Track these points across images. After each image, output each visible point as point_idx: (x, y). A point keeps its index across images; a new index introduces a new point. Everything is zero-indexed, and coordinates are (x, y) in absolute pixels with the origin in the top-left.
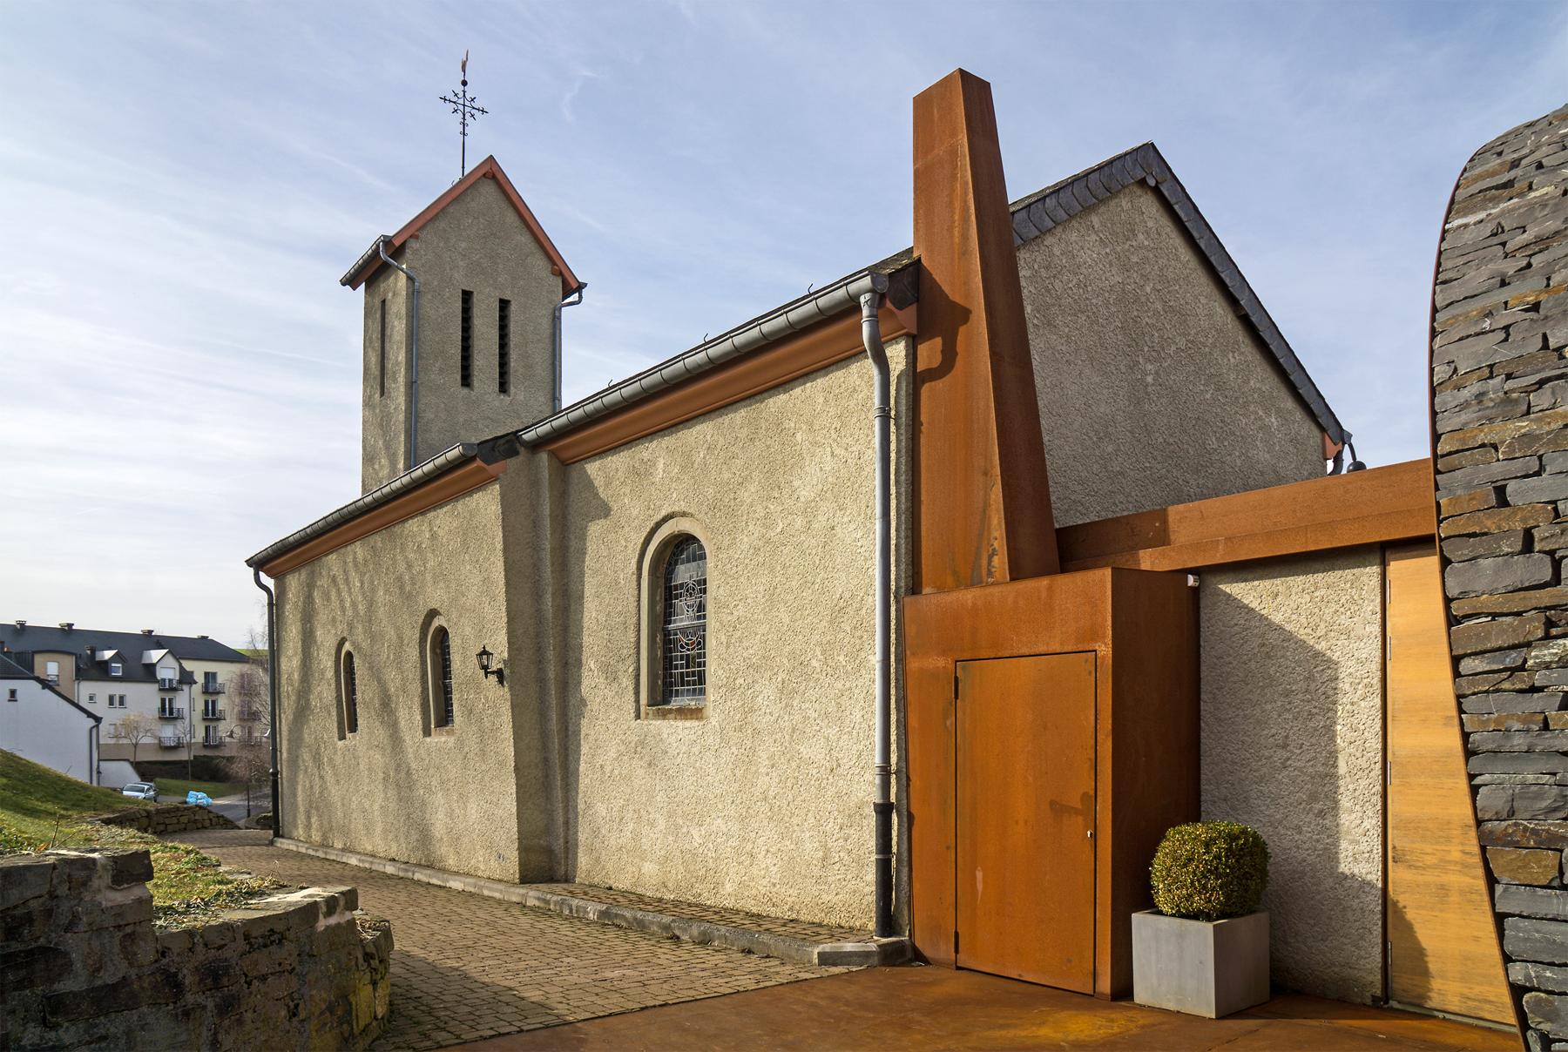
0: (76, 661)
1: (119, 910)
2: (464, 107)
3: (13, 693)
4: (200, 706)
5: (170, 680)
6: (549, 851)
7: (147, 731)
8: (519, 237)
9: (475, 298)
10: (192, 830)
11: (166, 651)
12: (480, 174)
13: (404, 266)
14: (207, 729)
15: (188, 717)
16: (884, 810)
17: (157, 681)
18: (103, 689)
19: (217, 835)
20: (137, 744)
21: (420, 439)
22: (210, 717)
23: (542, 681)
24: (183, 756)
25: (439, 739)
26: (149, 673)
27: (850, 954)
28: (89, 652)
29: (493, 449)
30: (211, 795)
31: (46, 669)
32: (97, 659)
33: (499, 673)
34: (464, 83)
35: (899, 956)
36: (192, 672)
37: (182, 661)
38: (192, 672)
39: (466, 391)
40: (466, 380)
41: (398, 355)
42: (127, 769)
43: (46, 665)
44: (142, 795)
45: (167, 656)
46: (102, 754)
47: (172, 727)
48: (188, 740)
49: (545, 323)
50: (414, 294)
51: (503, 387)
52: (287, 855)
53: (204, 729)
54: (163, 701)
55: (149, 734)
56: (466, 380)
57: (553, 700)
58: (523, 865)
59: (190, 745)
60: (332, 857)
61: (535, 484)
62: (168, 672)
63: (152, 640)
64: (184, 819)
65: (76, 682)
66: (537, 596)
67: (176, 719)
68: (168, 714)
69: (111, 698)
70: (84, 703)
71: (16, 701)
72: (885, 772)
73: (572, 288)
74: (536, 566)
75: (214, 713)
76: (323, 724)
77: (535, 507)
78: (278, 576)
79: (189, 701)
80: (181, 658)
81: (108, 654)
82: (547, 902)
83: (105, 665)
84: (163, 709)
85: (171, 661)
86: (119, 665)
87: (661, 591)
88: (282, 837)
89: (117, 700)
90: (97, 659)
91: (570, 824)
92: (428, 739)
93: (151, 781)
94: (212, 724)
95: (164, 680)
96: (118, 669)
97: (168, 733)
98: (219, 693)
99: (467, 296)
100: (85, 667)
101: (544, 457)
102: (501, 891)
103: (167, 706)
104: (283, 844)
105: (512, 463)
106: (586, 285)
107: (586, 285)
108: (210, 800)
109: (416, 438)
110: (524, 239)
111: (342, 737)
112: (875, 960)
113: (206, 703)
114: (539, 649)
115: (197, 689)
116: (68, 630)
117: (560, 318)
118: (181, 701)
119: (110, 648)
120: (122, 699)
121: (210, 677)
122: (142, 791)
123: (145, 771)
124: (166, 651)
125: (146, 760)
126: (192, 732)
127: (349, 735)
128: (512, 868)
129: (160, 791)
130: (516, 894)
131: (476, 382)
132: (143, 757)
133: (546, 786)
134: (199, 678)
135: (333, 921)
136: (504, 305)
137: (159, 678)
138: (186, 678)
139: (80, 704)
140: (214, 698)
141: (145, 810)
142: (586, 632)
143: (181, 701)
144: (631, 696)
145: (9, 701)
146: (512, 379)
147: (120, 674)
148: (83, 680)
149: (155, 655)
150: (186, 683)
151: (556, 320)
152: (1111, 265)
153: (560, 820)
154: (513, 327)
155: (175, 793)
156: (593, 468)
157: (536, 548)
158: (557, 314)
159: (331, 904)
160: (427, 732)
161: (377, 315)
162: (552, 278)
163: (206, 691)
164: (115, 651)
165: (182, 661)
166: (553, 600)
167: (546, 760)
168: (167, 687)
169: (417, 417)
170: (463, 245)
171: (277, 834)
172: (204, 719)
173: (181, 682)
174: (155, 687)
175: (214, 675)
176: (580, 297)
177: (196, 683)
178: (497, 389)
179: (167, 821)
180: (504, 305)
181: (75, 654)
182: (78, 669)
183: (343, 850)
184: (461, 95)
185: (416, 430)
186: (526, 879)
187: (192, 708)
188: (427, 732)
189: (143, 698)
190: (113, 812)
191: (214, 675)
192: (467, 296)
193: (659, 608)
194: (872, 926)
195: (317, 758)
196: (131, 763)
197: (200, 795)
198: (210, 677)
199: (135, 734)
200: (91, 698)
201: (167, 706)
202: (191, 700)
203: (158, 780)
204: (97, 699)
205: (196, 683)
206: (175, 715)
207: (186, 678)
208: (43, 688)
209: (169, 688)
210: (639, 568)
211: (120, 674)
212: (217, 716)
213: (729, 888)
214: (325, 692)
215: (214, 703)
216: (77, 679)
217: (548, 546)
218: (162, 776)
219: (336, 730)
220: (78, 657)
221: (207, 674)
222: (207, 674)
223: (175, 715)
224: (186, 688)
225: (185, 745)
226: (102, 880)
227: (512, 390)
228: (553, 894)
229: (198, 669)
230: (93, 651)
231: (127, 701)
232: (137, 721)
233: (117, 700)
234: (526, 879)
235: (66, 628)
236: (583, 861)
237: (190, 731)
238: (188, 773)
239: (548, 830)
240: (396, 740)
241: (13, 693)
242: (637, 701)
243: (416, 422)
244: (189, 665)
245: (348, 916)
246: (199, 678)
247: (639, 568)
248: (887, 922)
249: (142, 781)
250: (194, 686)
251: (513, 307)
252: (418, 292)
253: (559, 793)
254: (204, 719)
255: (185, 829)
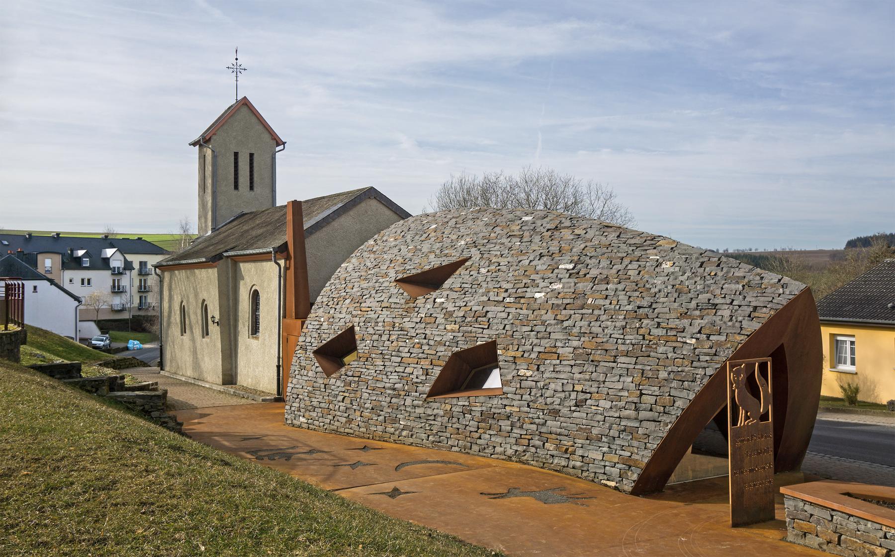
0: (62, 258)
1: (121, 383)
2: (237, 70)
3: (35, 288)
4: (136, 283)
5: (119, 268)
6: (231, 375)
7: (104, 302)
8: (257, 127)
9: (240, 155)
10: (130, 367)
11: (116, 249)
12: (241, 104)
13: (210, 146)
14: (141, 297)
15: (129, 291)
16: (278, 367)
17: (111, 269)
18: (78, 275)
19: (140, 369)
20: (98, 309)
21: (217, 213)
22: (143, 290)
23: (229, 325)
24: (126, 316)
25: (206, 340)
26: (105, 263)
27: (268, 399)
28: (69, 252)
29: (215, 258)
30: (142, 342)
31: (44, 263)
32: (74, 256)
33: (218, 322)
34: (237, 59)
35: (280, 399)
36: (132, 262)
37: (125, 255)
38: (132, 262)
39: (236, 192)
40: (236, 187)
41: (209, 181)
42: (93, 325)
43: (44, 261)
44: (102, 343)
45: (116, 253)
46: (81, 317)
47: (119, 297)
48: (129, 306)
49: (269, 160)
50: (214, 157)
51: (252, 188)
52: (165, 377)
53: (139, 281)
54: (114, 281)
55: (105, 304)
56: (236, 187)
57: (232, 331)
58: (223, 379)
59: (130, 309)
60: (177, 378)
61: (228, 267)
62: (117, 262)
63: (108, 241)
64: (127, 363)
65: (62, 271)
66: (228, 300)
67: (122, 292)
68: (117, 290)
69: (83, 280)
70: (67, 286)
71: (37, 292)
72: (279, 358)
73: (279, 142)
74: (228, 291)
75: (145, 288)
76: (175, 330)
77: (227, 274)
78: (163, 271)
79: (130, 281)
80: (124, 253)
81: (81, 253)
82: (224, 390)
83: (78, 260)
84: (114, 286)
85: (119, 256)
86: (88, 259)
87: (255, 303)
88: (164, 370)
89: (86, 282)
90: (74, 256)
91: (236, 367)
92: (203, 339)
93: (107, 333)
94: (144, 295)
95: (115, 268)
96: (86, 262)
97: (117, 301)
98: (148, 275)
99: (236, 155)
100: (67, 261)
101: (229, 260)
102: (216, 387)
103: (116, 285)
104: (162, 373)
105: (221, 262)
106: (286, 142)
107: (286, 142)
108: (141, 345)
109: (216, 213)
110: (261, 128)
111: (182, 335)
112: (273, 401)
113: (141, 281)
114: (229, 316)
115: (135, 273)
116: (57, 237)
117: (275, 158)
118: (125, 281)
119: (82, 249)
120: (89, 280)
121: (143, 264)
122: (102, 340)
123: (104, 326)
124: (116, 249)
125: (103, 319)
126: (131, 302)
127: (184, 334)
128: (220, 381)
129: (112, 339)
130: (222, 388)
131: (240, 188)
132: (102, 317)
133: (231, 357)
134: (136, 266)
135: (153, 387)
136: (251, 155)
137: (111, 267)
138: (128, 266)
139: (65, 287)
140: (145, 278)
141: (113, 360)
142: (240, 312)
143: (125, 281)
144: (247, 332)
145: (33, 292)
146: (255, 185)
147: (88, 265)
148: (67, 269)
149: (109, 252)
150: (129, 269)
151: (273, 159)
152: (356, 223)
153: (234, 366)
154: (255, 164)
155: (121, 341)
156: (241, 265)
157: (228, 286)
158: (274, 156)
159: (152, 384)
160: (203, 337)
161: (202, 158)
162: (272, 141)
163: (140, 273)
164: (85, 251)
165: (125, 255)
166: (232, 302)
167: (231, 348)
168: (116, 272)
169: (216, 205)
170: (234, 134)
171: (162, 369)
172: (139, 292)
173: (125, 269)
174: (110, 272)
175: (145, 263)
176: (284, 147)
177: (134, 269)
178: (249, 190)
179: (121, 364)
180: (251, 155)
181: (62, 254)
182: (63, 263)
183: (181, 375)
184: (235, 65)
185: (216, 210)
186: (224, 384)
187: (131, 285)
188: (203, 337)
189: (102, 280)
190: (101, 361)
191: (145, 263)
192: (236, 155)
193: (254, 308)
194: (276, 393)
195: (173, 342)
196: (95, 321)
197: (136, 342)
198: (143, 264)
199: (98, 304)
200: (71, 281)
201: (116, 285)
202: (131, 280)
203: (110, 332)
204: (74, 281)
205: (134, 269)
206: (121, 290)
207: (128, 266)
208: (51, 285)
209: (117, 273)
210: (249, 297)
211: (88, 265)
212: (147, 289)
213: (261, 385)
214: (176, 317)
215: (145, 280)
216: (62, 269)
217: (231, 286)
218: (113, 330)
219: (180, 332)
220: (63, 255)
221: (141, 263)
222: (141, 263)
223: (121, 290)
224: (128, 272)
225: (127, 309)
226: (119, 379)
227: (255, 189)
228: (231, 389)
229: (135, 259)
230: (72, 251)
231: (92, 282)
232: (99, 296)
233: (86, 282)
234: (224, 384)
235: (56, 236)
236: (239, 378)
237: (130, 299)
238: (128, 327)
239: (231, 369)
240: (193, 340)
241: (35, 288)
242: (249, 333)
243: (216, 207)
244: (130, 257)
245: (156, 386)
246: (136, 266)
247: (249, 297)
248: (279, 393)
249: (102, 334)
250: (133, 271)
251: (255, 156)
252: (216, 156)
253: (234, 358)
254: (139, 292)
255: (128, 367)
